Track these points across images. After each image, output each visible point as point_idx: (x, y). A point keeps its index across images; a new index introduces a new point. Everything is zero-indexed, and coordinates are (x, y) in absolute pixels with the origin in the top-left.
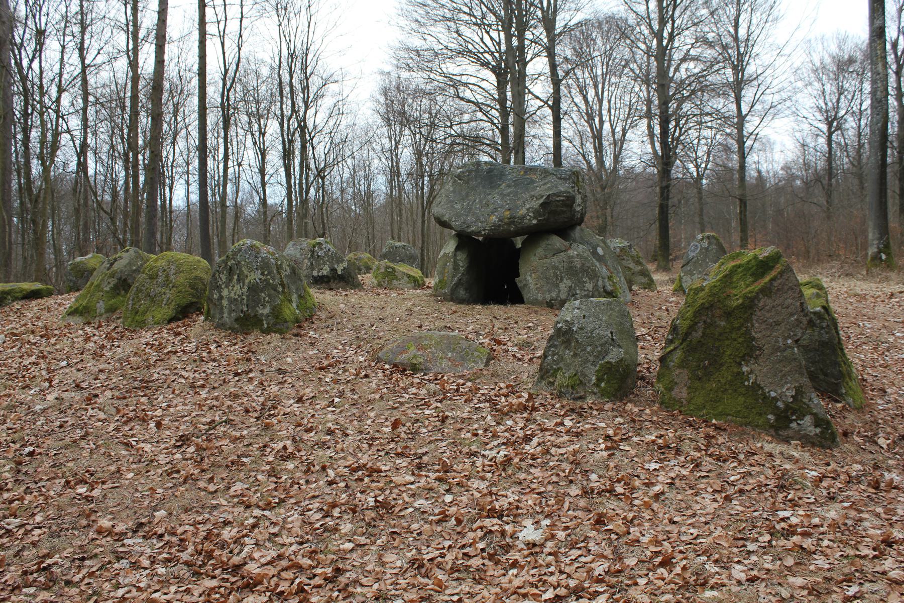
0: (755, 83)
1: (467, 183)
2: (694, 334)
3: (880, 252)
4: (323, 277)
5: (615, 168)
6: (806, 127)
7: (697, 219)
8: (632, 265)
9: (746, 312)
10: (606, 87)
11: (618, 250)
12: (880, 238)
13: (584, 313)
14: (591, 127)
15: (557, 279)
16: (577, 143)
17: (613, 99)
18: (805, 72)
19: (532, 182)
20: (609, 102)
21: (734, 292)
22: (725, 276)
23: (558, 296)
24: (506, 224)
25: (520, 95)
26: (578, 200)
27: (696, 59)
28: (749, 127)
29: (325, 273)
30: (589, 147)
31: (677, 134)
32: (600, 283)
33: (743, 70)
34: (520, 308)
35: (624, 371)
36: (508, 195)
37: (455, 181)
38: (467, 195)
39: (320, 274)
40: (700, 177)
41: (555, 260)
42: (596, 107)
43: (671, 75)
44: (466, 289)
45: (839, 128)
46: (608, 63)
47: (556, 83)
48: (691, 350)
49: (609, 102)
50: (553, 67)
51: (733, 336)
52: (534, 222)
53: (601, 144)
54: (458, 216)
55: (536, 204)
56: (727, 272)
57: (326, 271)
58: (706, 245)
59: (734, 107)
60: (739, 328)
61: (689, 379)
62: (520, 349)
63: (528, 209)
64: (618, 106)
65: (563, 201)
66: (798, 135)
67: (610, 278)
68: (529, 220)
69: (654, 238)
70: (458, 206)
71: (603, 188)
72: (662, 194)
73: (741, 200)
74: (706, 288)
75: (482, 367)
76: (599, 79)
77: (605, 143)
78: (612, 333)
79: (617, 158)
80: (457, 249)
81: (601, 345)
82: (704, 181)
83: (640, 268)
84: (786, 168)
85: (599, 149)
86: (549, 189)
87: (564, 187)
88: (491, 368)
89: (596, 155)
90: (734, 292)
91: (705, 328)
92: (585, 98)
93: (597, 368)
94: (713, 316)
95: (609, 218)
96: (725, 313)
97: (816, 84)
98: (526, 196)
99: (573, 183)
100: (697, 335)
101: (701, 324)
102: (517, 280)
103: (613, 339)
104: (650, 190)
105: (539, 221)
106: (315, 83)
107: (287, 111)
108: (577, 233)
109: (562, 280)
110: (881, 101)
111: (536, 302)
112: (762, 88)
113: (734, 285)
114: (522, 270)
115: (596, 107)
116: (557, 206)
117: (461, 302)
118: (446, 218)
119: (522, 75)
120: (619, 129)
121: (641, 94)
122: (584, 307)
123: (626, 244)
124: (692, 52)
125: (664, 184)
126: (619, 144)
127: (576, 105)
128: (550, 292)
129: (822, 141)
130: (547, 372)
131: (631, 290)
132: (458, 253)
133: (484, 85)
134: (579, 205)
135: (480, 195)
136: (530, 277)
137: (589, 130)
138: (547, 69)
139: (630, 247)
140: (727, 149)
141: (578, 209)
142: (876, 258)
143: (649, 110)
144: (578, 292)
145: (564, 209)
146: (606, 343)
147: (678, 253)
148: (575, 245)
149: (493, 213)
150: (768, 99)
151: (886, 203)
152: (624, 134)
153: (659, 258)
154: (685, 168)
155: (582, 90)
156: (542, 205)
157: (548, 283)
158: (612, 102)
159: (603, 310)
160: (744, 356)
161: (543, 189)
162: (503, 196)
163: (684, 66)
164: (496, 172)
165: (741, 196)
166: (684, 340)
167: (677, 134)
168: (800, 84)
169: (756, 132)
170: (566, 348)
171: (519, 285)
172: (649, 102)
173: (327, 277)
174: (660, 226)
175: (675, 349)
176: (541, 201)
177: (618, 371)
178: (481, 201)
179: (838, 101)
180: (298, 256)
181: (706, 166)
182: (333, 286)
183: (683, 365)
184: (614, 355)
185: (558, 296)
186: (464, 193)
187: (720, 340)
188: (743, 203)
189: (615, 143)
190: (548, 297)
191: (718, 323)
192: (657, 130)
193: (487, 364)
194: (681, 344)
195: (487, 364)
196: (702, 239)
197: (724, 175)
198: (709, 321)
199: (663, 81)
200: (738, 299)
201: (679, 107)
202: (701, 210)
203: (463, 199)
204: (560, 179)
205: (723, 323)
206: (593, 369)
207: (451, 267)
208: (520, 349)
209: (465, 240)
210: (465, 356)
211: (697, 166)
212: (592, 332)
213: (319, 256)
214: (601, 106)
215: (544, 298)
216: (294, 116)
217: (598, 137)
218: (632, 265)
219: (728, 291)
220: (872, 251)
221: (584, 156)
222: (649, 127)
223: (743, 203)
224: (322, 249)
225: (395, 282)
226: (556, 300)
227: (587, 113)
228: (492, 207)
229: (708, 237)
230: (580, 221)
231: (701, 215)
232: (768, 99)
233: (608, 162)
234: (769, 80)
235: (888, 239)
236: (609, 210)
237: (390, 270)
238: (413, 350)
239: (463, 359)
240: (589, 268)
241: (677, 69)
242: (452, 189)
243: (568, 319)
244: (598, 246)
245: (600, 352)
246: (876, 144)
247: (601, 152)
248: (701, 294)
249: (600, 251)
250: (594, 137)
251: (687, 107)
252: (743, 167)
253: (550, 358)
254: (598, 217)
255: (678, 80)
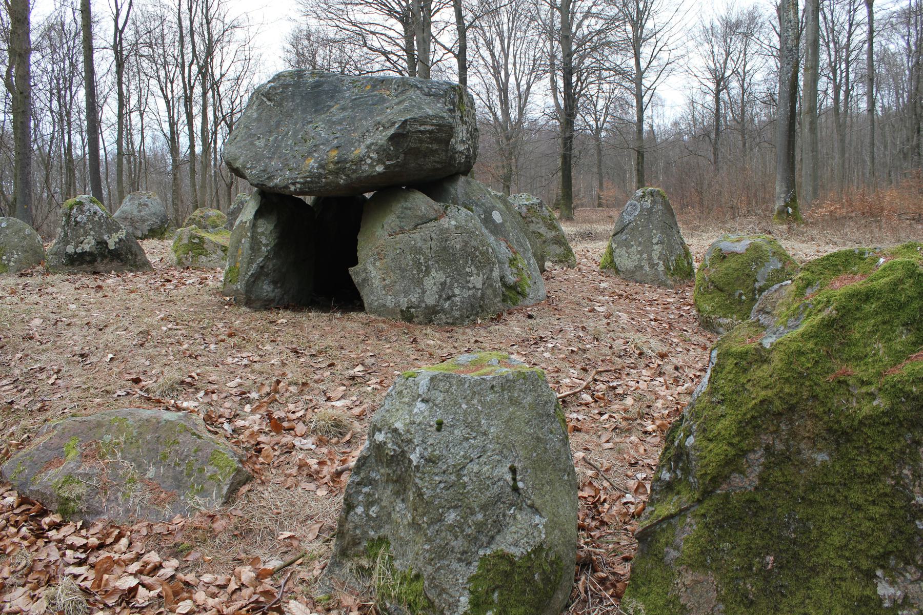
0: (653, 40)
1: (280, 105)
2: (736, 479)
3: (786, 206)
4: (84, 254)
5: (519, 120)
6: (696, 84)
7: (596, 170)
8: (543, 230)
9: (897, 437)
10: (512, 42)
11: (524, 209)
12: (788, 192)
13: (439, 415)
14: (497, 80)
15: (419, 270)
16: (484, 97)
17: (518, 53)
18: (696, 32)
19: (382, 100)
20: (515, 56)
21: (858, 371)
22: (829, 324)
23: (421, 300)
24: (330, 172)
25: (424, 41)
26: (461, 132)
27: (597, 16)
28: (646, 83)
29: (87, 248)
30: (496, 99)
31: (578, 88)
32: (496, 274)
33: (642, 27)
34: (349, 325)
35: (546, 579)
36: (340, 122)
37: (262, 102)
38: (278, 125)
39: (79, 250)
40: (599, 130)
41: (417, 236)
42: (502, 62)
43: (574, 30)
44: (275, 283)
45: (726, 87)
46: (513, 19)
47: (462, 31)
48: (728, 519)
49: (515, 56)
50: (460, 17)
51: (856, 496)
52: (380, 169)
53: (506, 97)
54: (257, 159)
55: (381, 137)
56: (830, 312)
57: (88, 245)
58: (648, 204)
59: (632, 62)
60: (872, 479)
61: (721, 599)
62: (321, 443)
63: (368, 147)
64: (523, 60)
65: (431, 132)
66: (688, 92)
67: (512, 262)
68: (371, 165)
69: (556, 188)
70: (260, 143)
71: (508, 139)
72: (565, 144)
73: (639, 152)
74: (776, 357)
75: (217, 507)
76: (506, 34)
77: (511, 96)
78: (513, 470)
79: (521, 110)
80: (259, 214)
81: (484, 508)
82: (603, 134)
83: (553, 233)
84: (676, 124)
85: (505, 102)
86: (406, 110)
87: (433, 109)
88: (237, 510)
89: (502, 108)
90: (858, 371)
91: (767, 467)
92: (493, 54)
93: (474, 569)
94: (793, 434)
95: (513, 168)
96: (829, 430)
97: (706, 44)
98: (368, 123)
99: (453, 103)
100: (745, 482)
101: (757, 457)
102: (351, 270)
103: (515, 489)
104: (552, 141)
105: (387, 167)
106: (217, 27)
107: (188, 57)
108: (460, 187)
109: (428, 272)
110: (791, 50)
111: (381, 311)
112: (660, 44)
113: (854, 351)
114: (361, 254)
115: (502, 62)
116: (421, 141)
117: (267, 305)
118: (238, 164)
119: (427, 23)
120: (523, 82)
121: (545, 50)
122: (440, 397)
123: (535, 200)
124: (594, 10)
125: (568, 135)
126: (524, 97)
127: (483, 59)
128: (406, 293)
129: (710, 99)
130: (356, 542)
131: (543, 270)
132: (260, 222)
133: (391, 33)
134: (463, 142)
135: (296, 124)
136: (373, 269)
137: (494, 82)
138: (453, 19)
139: (541, 205)
140: (623, 103)
141: (461, 148)
142: (782, 212)
143: (552, 64)
144: (457, 291)
145: (435, 147)
146: (499, 498)
147: (579, 202)
148: (452, 209)
149: (310, 153)
150: (664, 56)
151: (793, 157)
152: (529, 88)
153: (563, 207)
154: (584, 120)
155: (489, 44)
156: (392, 138)
157: (403, 277)
158: (518, 56)
159: (492, 404)
160: (886, 555)
161: (396, 112)
162: (331, 124)
163: (586, 23)
164: (326, 87)
165: (639, 149)
166: (707, 494)
167: (578, 88)
168: (691, 44)
169: (653, 87)
170: (397, 494)
171: (356, 279)
172: (553, 56)
173: (90, 254)
174: (563, 176)
175: (682, 513)
176: (392, 131)
177: (529, 581)
178: (295, 134)
179: (725, 62)
180: (135, 213)
181: (605, 119)
182: (101, 267)
183: (702, 560)
184: (518, 536)
185: (421, 300)
186: (273, 122)
187: (811, 504)
188: (640, 154)
189: (520, 97)
190: (404, 302)
191: (806, 454)
192: (561, 83)
193: (230, 498)
194: (699, 501)
195: (230, 498)
196: (643, 196)
197: (621, 127)
198: (779, 446)
199: (566, 38)
200: (872, 396)
201: (581, 62)
202: (600, 161)
203: (270, 132)
204: (429, 95)
205: (821, 457)
206: (464, 573)
207: (247, 245)
208: (321, 443)
209: (273, 201)
210: (183, 477)
211: (597, 120)
212: (459, 470)
213: (77, 223)
214: (506, 60)
215: (397, 305)
216: (195, 61)
217: (503, 90)
218: (543, 230)
219: (839, 367)
220: (779, 204)
221: (490, 108)
222: (553, 82)
223: (640, 154)
224: (82, 212)
225: (203, 259)
226: (418, 307)
227: (493, 67)
228: (310, 143)
229: (652, 194)
230: (466, 170)
231: (599, 166)
232: (664, 56)
233: (514, 114)
234: (665, 39)
235: (794, 192)
236: (514, 161)
237: (196, 241)
238: (71, 462)
239: (179, 483)
240: (476, 249)
241: (579, 26)
242: (255, 115)
243: (399, 425)
244: (494, 208)
245: (480, 527)
246: (786, 95)
247: (507, 104)
248: (761, 372)
249: (497, 217)
250: (500, 90)
251: (588, 62)
252: (641, 120)
253: (360, 510)
254: (503, 167)
255: (581, 37)
